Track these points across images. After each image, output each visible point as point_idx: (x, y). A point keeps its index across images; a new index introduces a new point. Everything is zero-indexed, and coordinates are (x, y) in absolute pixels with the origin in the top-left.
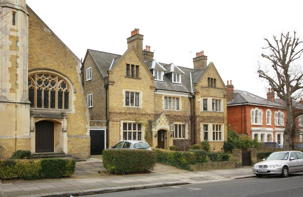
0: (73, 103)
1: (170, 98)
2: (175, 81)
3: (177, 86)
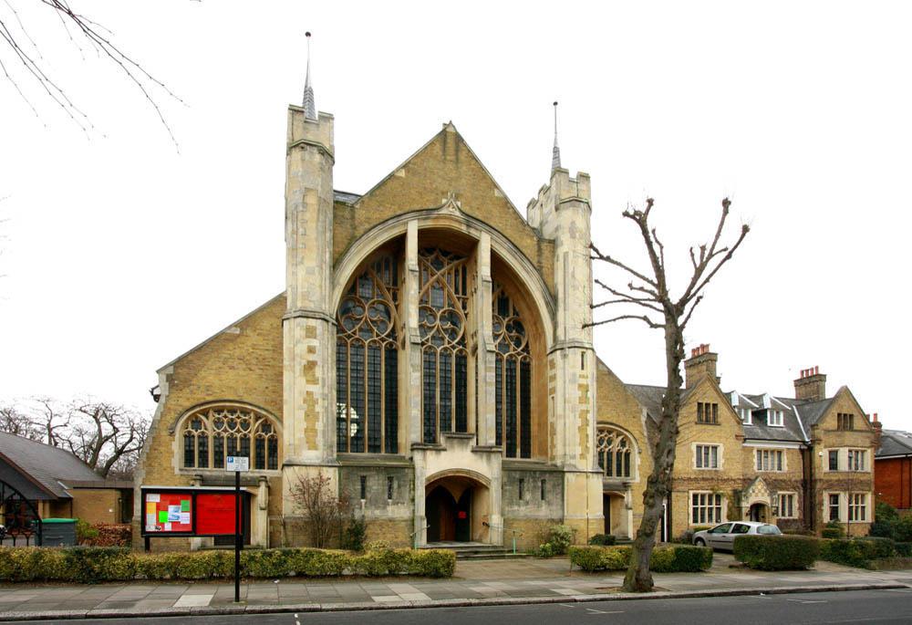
0: (637, 468)
1: (766, 451)
2: (772, 422)
3: (778, 431)
